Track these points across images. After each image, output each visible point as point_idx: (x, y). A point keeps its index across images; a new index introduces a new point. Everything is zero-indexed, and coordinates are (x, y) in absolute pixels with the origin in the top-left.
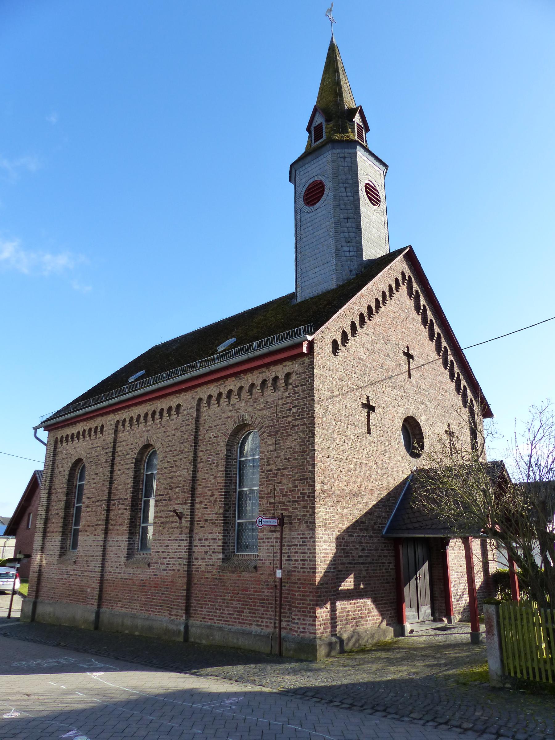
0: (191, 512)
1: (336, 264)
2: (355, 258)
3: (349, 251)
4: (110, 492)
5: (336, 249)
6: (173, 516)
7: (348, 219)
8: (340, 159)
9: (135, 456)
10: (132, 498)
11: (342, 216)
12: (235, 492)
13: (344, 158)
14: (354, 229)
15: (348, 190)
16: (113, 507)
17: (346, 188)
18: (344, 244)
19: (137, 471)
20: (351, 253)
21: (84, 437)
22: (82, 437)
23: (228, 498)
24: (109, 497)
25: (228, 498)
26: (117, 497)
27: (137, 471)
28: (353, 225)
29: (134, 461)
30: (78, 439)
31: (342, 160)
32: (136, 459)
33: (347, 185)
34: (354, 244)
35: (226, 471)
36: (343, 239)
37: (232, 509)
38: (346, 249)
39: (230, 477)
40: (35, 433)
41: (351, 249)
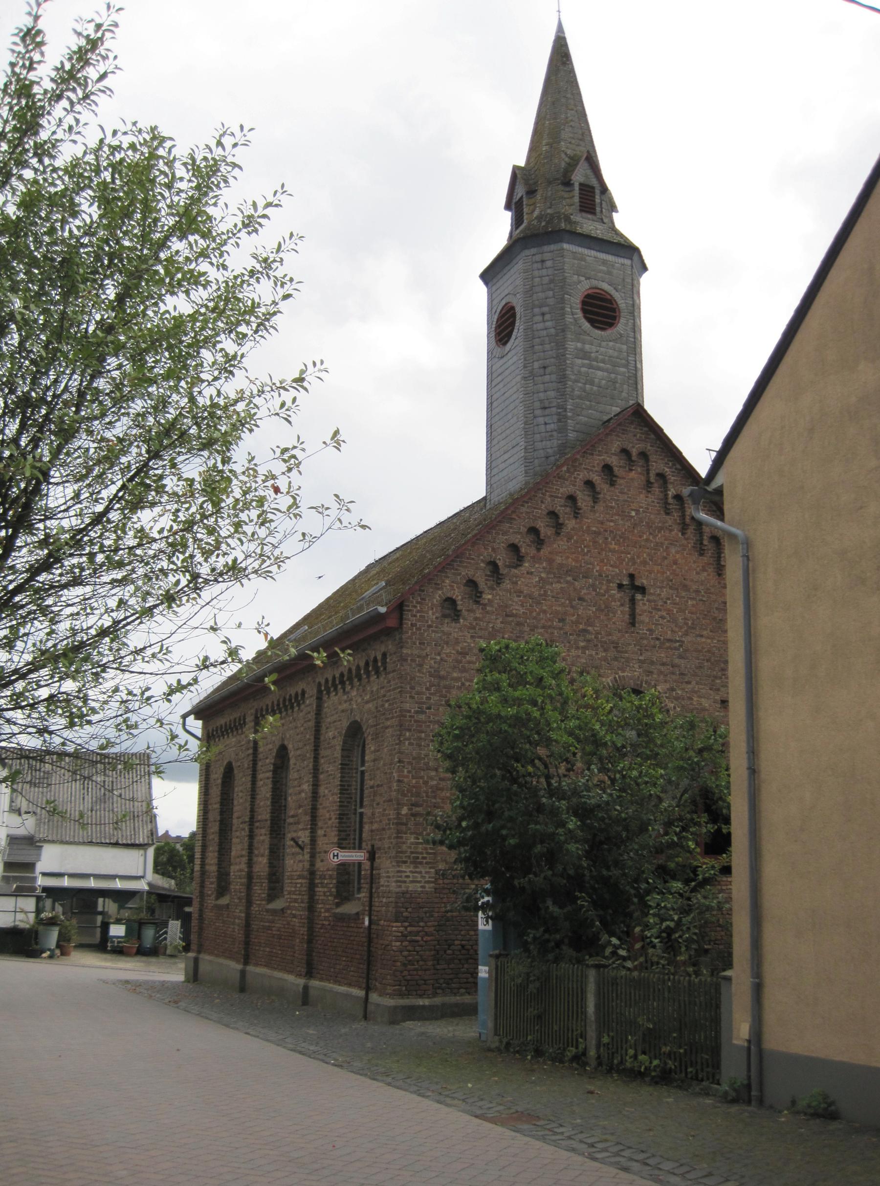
0: (311, 840)
1: (525, 448)
2: (555, 433)
3: (546, 424)
4: (252, 811)
5: (526, 423)
6: (292, 846)
7: (545, 368)
8: (535, 266)
9: (273, 761)
10: (272, 820)
11: (536, 365)
12: (355, 814)
13: (543, 261)
14: (554, 384)
15: (547, 317)
16: (257, 831)
17: (543, 314)
18: (538, 412)
19: (278, 782)
20: (548, 426)
21: (360, 680)
22: (356, 680)
23: (345, 823)
24: (252, 818)
25: (345, 823)
26: (259, 817)
27: (278, 782)
28: (554, 377)
29: (272, 768)
30: (336, 689)
31: (539, 265)
32: (274, 764)
33: (545, 309)
34: (554, 410)
35: (341, 785)
36: (537, 404)
37: (352, 837)
38: (541, 420)
39: (349, 794)
40: (184, 724)
41: (547, 419)
